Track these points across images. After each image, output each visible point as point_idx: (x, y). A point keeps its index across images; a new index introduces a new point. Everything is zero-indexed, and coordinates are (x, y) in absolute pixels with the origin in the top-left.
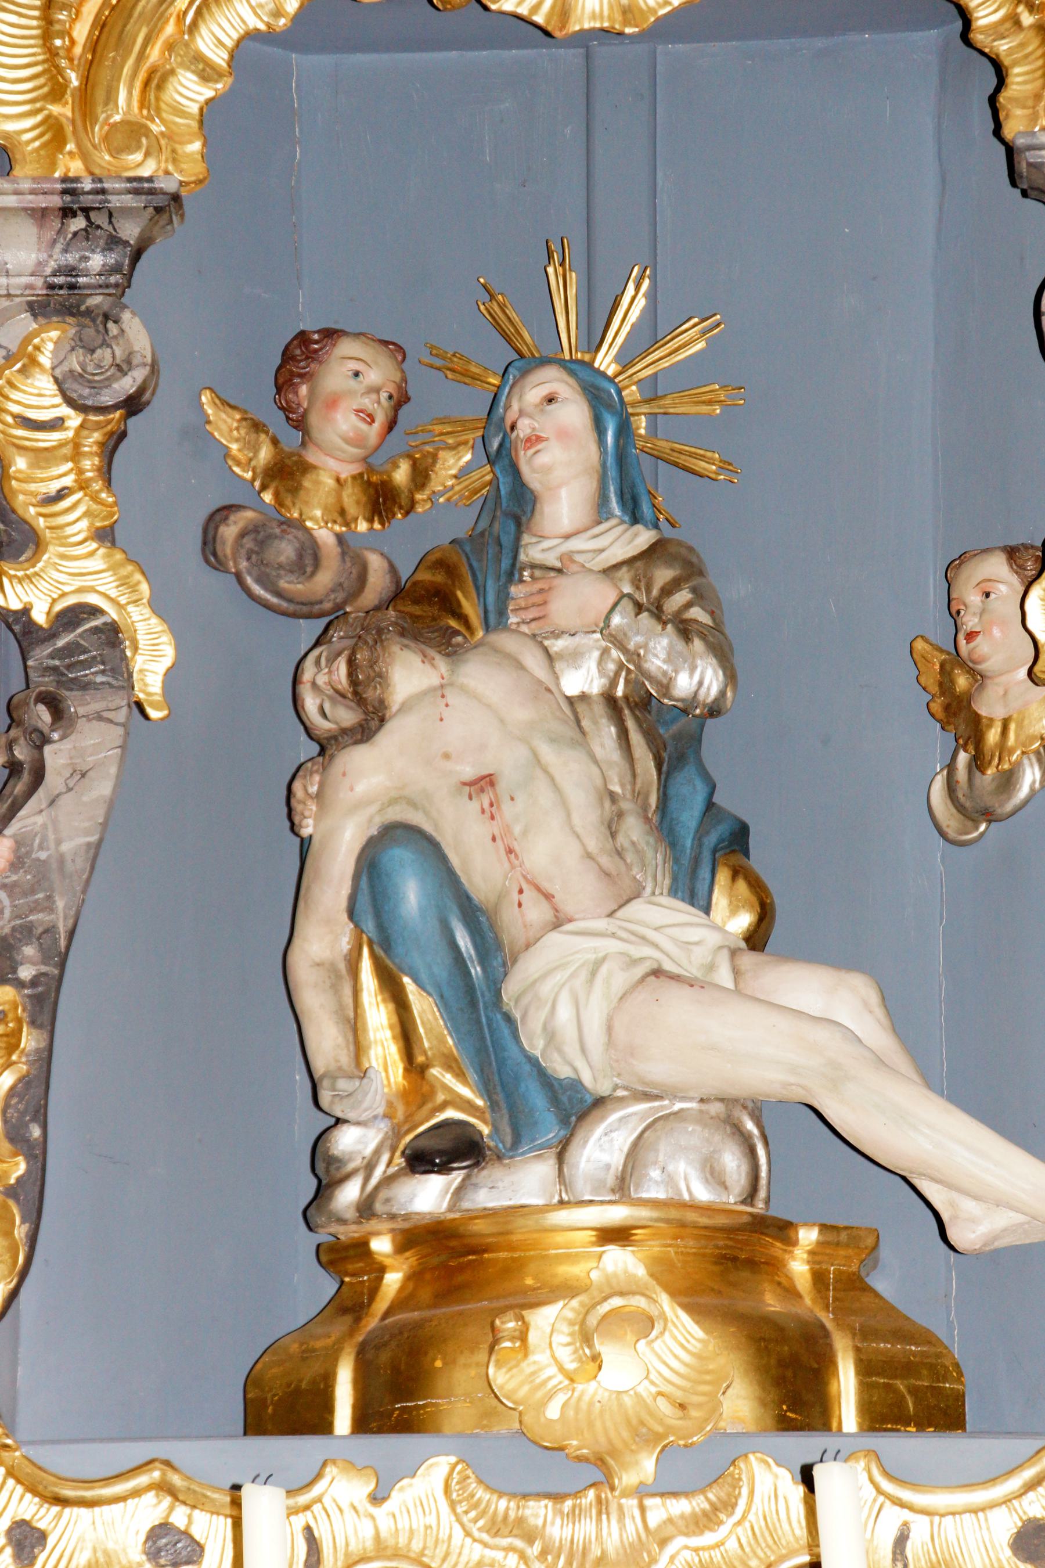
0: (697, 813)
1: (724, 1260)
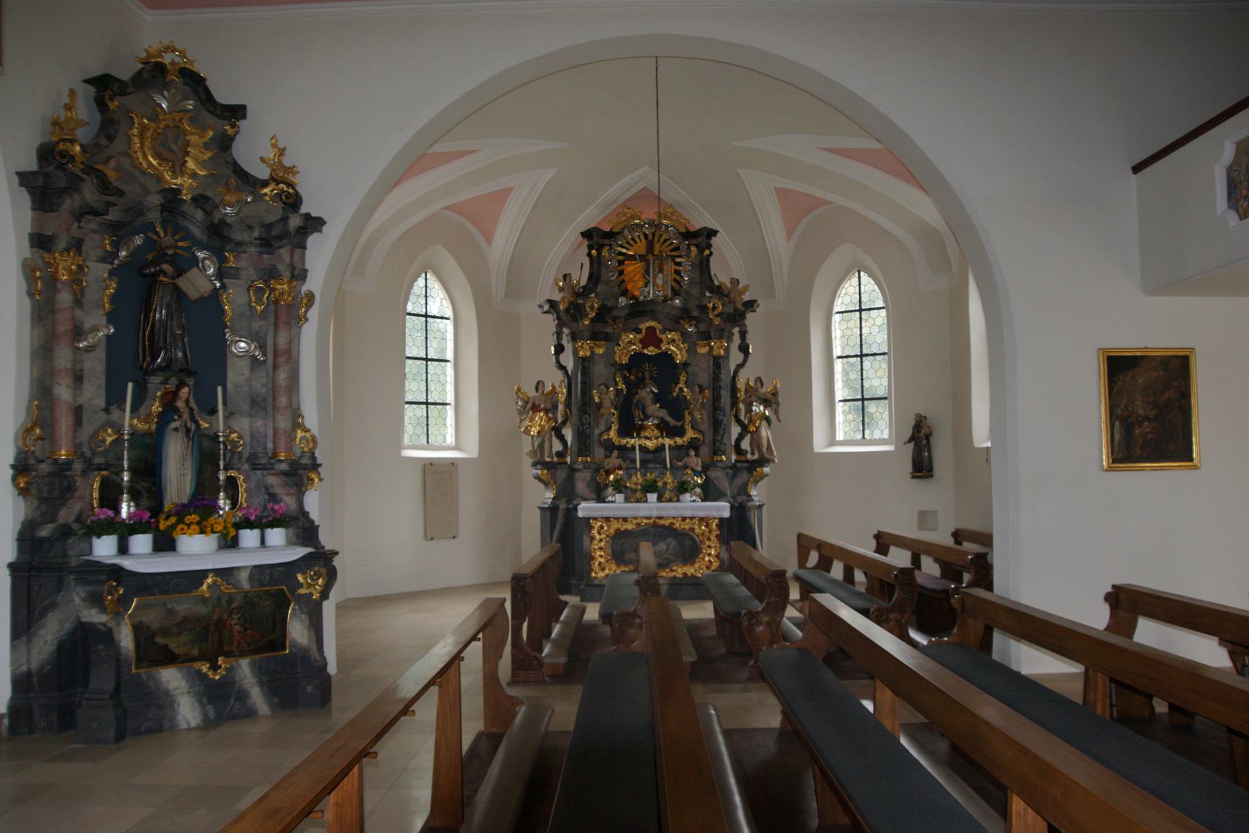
0: (657, 398)
1: (657, 426)
